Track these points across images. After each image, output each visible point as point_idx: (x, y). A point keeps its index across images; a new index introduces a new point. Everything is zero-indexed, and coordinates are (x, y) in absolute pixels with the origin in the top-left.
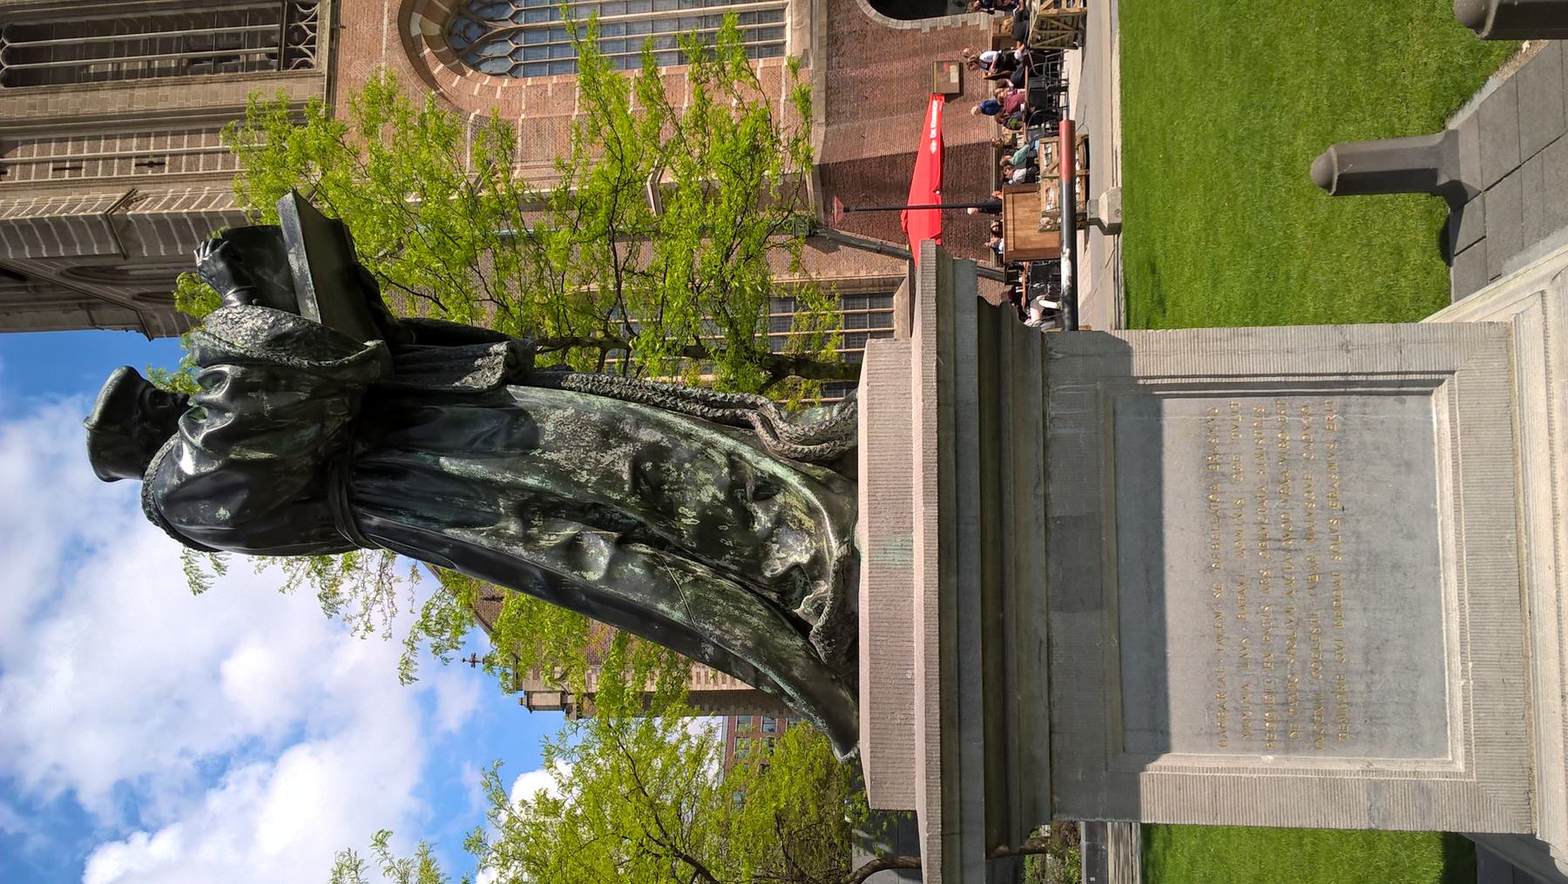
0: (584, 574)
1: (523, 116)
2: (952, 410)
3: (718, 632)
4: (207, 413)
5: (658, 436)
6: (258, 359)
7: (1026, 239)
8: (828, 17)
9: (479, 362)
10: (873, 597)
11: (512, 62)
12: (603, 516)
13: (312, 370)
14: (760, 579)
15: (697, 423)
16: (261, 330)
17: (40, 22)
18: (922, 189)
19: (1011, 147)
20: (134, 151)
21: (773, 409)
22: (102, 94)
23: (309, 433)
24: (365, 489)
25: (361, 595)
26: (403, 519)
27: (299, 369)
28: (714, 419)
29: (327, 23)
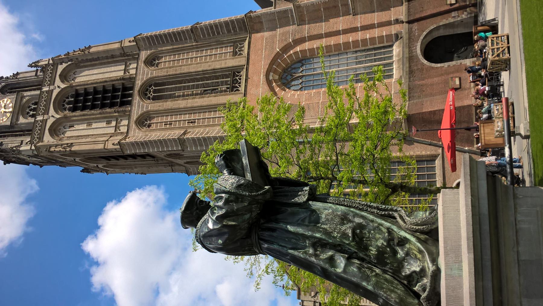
0: (336, 269)
1: (304, 103)
2: (478, 217)
3: (385, 295)
4: (217, 209)
5: (361, 221)
6: (233, 192)
7: (489, 140)
8: (409, 64)
9: (300, 193)
10: (447, 287)
11: (300, 86)
12: (342, 249)
13: (249, 196)
14: (400, 276)
15: (376, 217)
16: (235, 183)
17: (163, 81)
18: (446, 123)
19: (482, 106)
20: (187, 118)
21: (404, 212)
22: (179, 102)
23: (247, 216)
24: (264, 235)
25: (250, 262)
26: (275, 246)
27: (245, 196)
28: (382, 215)
29: (244, 77)
